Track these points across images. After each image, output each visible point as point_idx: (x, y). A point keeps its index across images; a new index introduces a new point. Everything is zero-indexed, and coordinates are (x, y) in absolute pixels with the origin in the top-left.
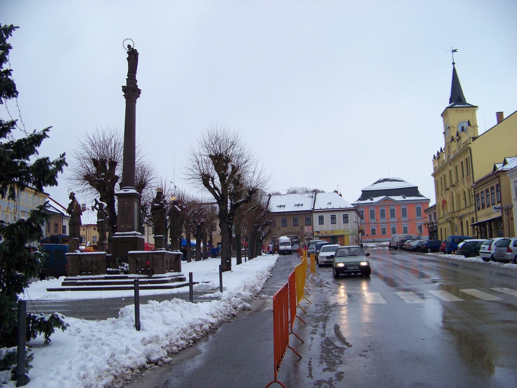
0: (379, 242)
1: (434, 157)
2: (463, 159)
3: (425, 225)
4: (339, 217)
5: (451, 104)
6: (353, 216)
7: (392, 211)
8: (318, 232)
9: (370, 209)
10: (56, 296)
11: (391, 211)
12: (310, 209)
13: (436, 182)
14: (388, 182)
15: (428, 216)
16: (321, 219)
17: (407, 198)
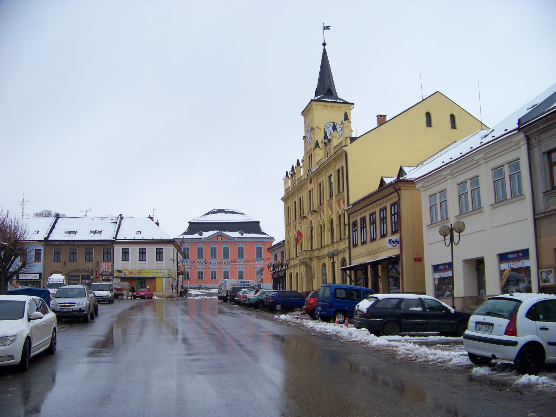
0: (206, 288)
1: (287, 176)
2: (332, 171)
3: (269, 267)
4: (151, 251)
5: (317, 98)
6: (169, 252)
7: (226, 251)
8: (120, 271)
9: (197, 247)
10: (329, 275)
11: (224, 250)
12: (111, 238)
13: (287, 210)
14: (223, 214)
15: (273, 257)
16: (125, 253)
17: (246, 235)
